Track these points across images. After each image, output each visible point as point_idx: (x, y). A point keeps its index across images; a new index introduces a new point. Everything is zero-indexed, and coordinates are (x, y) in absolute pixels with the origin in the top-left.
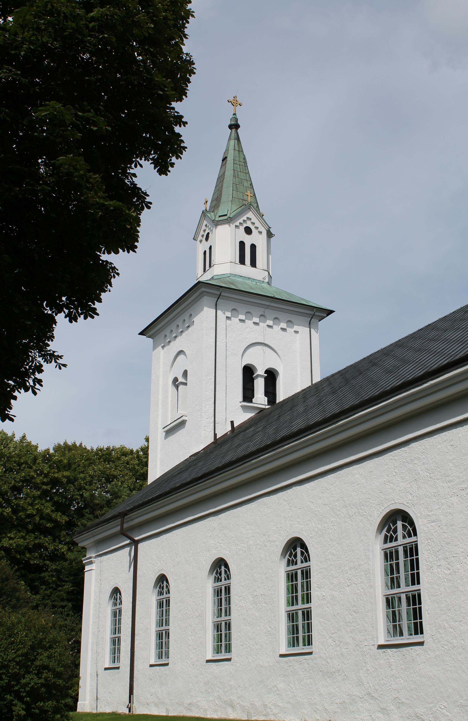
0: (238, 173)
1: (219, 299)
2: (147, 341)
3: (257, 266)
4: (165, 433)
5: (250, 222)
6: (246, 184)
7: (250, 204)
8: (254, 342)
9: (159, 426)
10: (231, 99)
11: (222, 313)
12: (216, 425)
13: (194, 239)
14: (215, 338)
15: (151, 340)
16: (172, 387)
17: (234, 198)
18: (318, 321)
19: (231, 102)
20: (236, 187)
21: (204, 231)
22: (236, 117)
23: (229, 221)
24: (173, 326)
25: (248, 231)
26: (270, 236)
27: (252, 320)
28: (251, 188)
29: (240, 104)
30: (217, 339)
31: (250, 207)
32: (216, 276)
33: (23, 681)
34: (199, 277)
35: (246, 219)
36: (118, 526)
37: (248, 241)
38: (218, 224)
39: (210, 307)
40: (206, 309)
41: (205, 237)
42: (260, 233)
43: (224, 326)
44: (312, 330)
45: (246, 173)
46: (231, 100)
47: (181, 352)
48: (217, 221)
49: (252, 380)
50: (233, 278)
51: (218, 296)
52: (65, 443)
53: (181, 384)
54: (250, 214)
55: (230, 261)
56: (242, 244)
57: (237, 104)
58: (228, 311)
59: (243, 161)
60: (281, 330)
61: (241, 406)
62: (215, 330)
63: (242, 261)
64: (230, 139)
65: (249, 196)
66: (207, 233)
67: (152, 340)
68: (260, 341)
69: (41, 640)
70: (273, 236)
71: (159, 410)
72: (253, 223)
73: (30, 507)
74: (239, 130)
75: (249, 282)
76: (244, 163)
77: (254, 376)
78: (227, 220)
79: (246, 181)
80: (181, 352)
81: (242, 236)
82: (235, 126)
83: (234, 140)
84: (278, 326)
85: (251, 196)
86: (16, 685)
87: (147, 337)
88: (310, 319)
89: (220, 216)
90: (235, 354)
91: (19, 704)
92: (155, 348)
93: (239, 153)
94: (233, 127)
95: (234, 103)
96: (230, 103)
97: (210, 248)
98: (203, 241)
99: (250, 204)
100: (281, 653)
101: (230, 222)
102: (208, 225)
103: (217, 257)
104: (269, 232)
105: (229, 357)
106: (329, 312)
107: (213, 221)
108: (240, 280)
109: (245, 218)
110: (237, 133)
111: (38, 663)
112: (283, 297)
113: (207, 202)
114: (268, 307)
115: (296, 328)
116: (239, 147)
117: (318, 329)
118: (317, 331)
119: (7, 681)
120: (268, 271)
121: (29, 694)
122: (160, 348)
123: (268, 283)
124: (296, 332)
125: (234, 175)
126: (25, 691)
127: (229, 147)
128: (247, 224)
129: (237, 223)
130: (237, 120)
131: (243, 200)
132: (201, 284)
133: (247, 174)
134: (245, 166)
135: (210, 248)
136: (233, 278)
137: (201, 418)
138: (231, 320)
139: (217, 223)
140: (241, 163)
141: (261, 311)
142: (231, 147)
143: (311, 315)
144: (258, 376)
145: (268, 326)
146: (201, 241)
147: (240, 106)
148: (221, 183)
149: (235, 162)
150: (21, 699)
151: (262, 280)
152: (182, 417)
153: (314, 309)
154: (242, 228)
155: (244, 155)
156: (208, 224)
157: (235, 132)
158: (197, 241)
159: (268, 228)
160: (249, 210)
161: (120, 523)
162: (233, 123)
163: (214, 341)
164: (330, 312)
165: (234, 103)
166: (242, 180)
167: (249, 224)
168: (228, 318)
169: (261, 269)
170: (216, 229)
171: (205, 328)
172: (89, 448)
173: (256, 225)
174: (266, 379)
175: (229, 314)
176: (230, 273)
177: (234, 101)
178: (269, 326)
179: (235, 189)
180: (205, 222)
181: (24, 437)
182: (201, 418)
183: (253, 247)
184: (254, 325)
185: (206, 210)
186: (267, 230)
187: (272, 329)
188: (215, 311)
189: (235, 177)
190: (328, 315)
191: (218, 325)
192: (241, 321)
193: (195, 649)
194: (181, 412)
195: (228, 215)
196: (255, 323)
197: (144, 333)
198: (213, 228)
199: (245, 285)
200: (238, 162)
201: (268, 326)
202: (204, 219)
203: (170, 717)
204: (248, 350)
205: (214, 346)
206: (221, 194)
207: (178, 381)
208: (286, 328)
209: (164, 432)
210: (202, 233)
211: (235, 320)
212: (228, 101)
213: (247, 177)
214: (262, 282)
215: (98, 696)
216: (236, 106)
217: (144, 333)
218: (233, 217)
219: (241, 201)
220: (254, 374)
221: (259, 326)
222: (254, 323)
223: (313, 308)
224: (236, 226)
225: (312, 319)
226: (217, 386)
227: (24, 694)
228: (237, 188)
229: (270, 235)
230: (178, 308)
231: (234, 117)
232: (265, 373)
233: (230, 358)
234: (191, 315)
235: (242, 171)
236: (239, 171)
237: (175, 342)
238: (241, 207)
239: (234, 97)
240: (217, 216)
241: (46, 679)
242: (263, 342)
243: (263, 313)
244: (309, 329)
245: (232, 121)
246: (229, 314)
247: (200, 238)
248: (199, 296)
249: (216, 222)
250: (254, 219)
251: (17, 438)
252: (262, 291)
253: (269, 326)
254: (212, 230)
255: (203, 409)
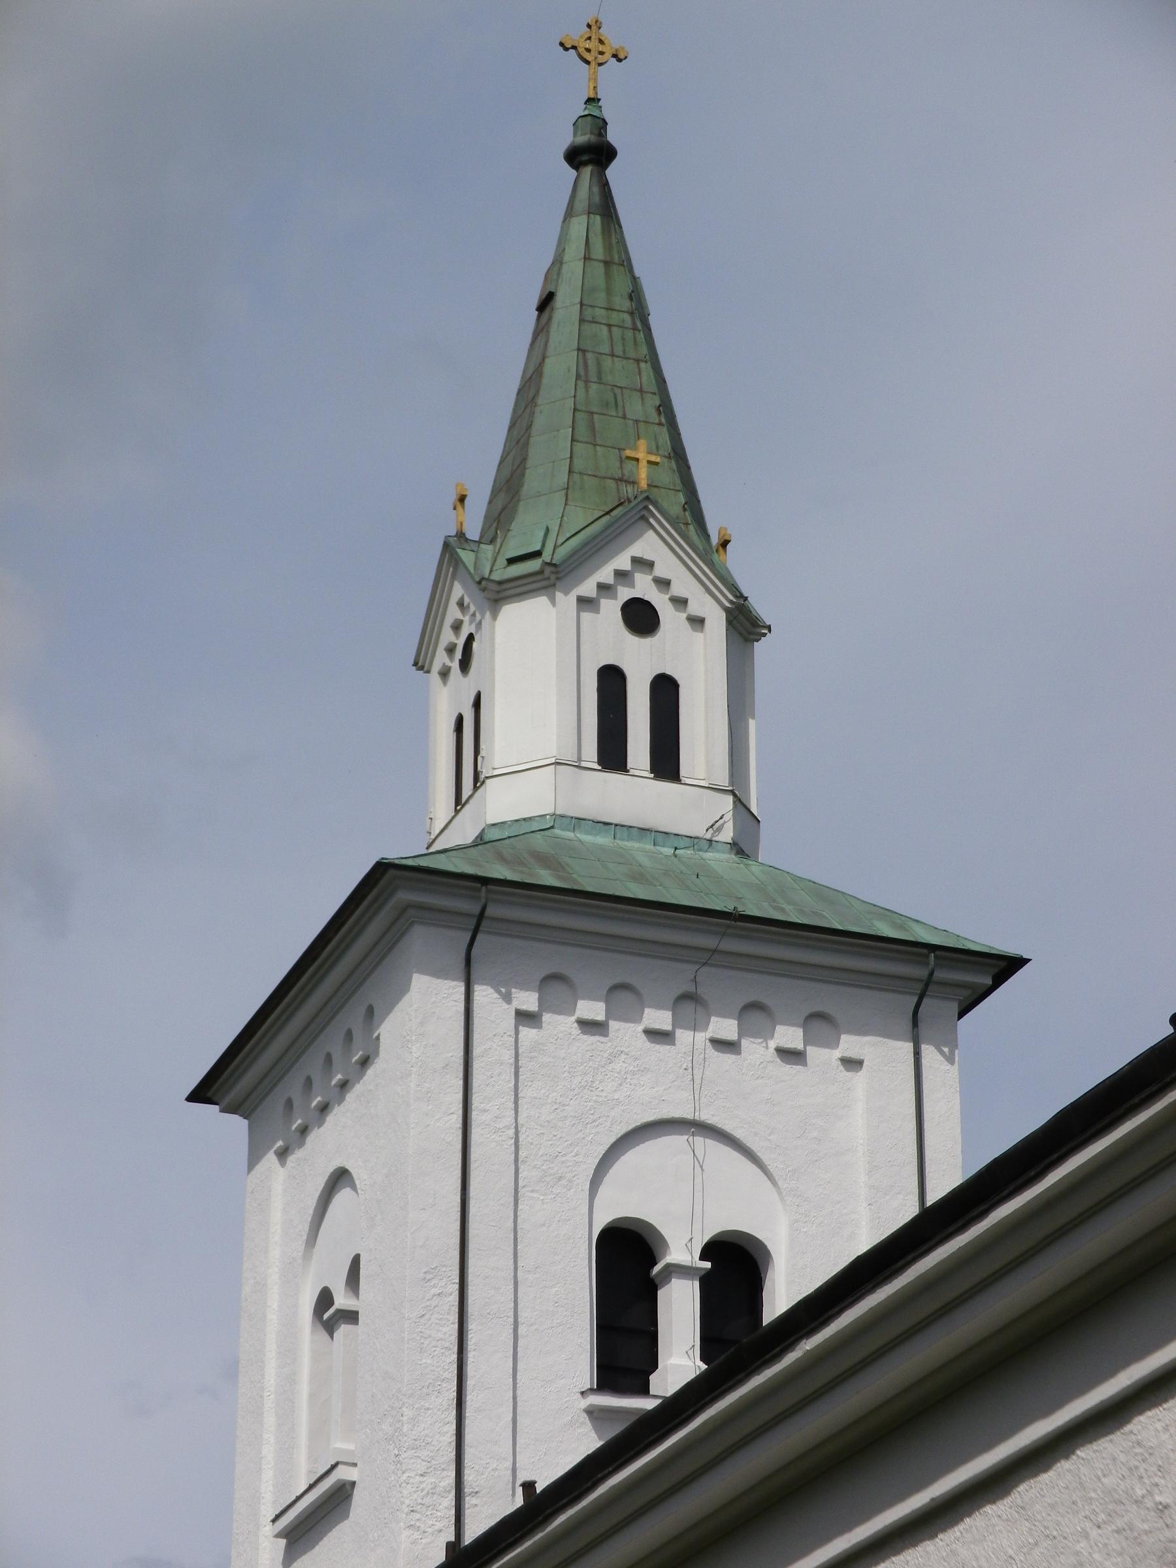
0: (599, 365)
1: (479, 937)
3: (684, 771)
4: (284, 1541)
5: (651, 577)
6: (637, 408)
7: (647, 498)
9: (262, 1507)
10: (577, 33)
11: (496, 995)
12: (469, 1501)
13: (415, 664)
14: (460, 1112)
15: (237, 1125)
16: (313, 1332)
17: (576, 477)
18: (954, 1008)
19: (574, 47)
21: (457, 627)
22: (596, 113)
23: (549, 578)
24: (312, 1064)
26: (750, 633)
27: (638, 1019)
28: (660, 424)
29: (615, 56)
30: (475, 1115)
31: (645, 512)
32: (493, 829)
34: (437, 832)
38: (502, 595)
39: (440, 973)
40: (419, 982)
41: (458, 654)
42: (697, 622)
43: (509, 1056)
44: (928, 1051)
45: (638, 361)
48: (500, 583)
49: (648, 1292)
50: (570, 835)
51: (474, 921)
53: (344, 1317)
54: (648, 545)
55: (553, 760)
57: (602, 53)
58: (524, 986)
59: (626, 304)
60: (778, 1060)
61: (591, 1412)
62: (461, 1075)
64: (570, 213)
65: (643, 464)
66: (466, 636)
67: (246, 1122)
68: (677, 1113)
70: (764, 635)
71: (266, 1436)
72: (663, 584)
75: (638, 848)
76: (632, 314)
77: (657, 1269)
78: (540, 577)
79: (637, 395)
80: (340, 1178)
83: (585, 217)
84: (766, 1041)
85: (649, 462)
87: (222, 1111)
88: (915, 999)
89: (512, 561)
90: (560, 1178)
93: (608, 275)
94: (585, 158)
95: (588, 50)
96: (572, 51)
97: (477, 704)
98: (452, 671)
99: (647, 498)
101: (554, 585)
102: (467, 600)
104: (741, 617)
105: (532, 1191)
106: (1003, 964)
107: (479, 583)
108: (602, 840)
109: (622, 562)
112: (783, 910)
114: (710, 958)
115: (850, 1044)
116: (608, 247)
117: (956, 1046)
118: (952, 1053)
120: (732, 792)
122: (271, 1158)
123: (738, 849)
125: (582, 373)
127: (564, 249)
128: (633, 587)
129: (588, 588)
130: (601, 125)
131: (621, 480)
132: (392, 872)
133: (643, 365)
134: (635, 329)
135: (477, 704)
136: (570, 835)
137: (399, 1473)
140: (615, 318)
141: (680, 978)
142: (575, 250)
143: (919, 980)
144: (674, 1270)
146: (445, 674)
147: (620, 60)
148: (528, 411)
149: (588, 313)
151: (699, 830)
152: (333, 1467)
153: (927, 956)
154: (611, 609)
155: (635, 279)
156: (465, 596)
157: (595, 180)
158: (428, 672)
159: (731, 597)
160: (642, 524)
162: (582, 139)
163: (459, 1124)
166: (618, 391)
167: (643, 587)
168: (525, 1018)
169: (702, 783)
170: (495, 616)
171: (414, 1069)
173: (677, 590)
174: (707, 1282)
175: (528, 1000)
176: (551, 811)
178: (720, 1044)
179: (582, 431)
180: (458, 591)
182: (399, 1473)
184: (648, 1044)
185: (461, 535)
186: (727, 610)
187: (733, 1057)
188: (461, 988)
189: (587, 382)
190: (1000, 979)
191: (477, 1051)
192: (589, 1026)
194: (342, 1445)
195: (546, 556)
197: (209, 1094)
198: (483, 616)
199: (611, 866)
200: (600, 313)
202: (454, 577)
204: (623, 1158)
205: (459, 1146)
206: (524, 460)
207: (331, 1303)
208: (800, 1046)
209: (278, 1536)
210: (447, 636)
211: (559, 1025)
212: (562, 44)
213: (644, 378)
214: (705, 845)
216: (600, 65)
217: (209, 1094)
218: (564, 561)
219: (611, 484)
220: (654, 1263)
221: (674, 1044)
223: (925, 951)
225: (926, 1001)
230: (321, 980)
231: (586, 113)
233: (535, 1195)
234: (370, 1011)
235: (618, 350)
236: (607, 351)
237: (322, 1129)
238: (608, 513)
239: (589, 26)
240: (501, 561)
242: (690, 1116)
243: (690, 988)
244: (909, 1046)
245: (579, 133)
246: (528, 1000)
247: (441, 659)
248: (393, 924)
249: (496, 587)
250: (667, 564)
252: (688, 888)
253: (720, 1044)
254: (480, 623)
255: (405, 1429)
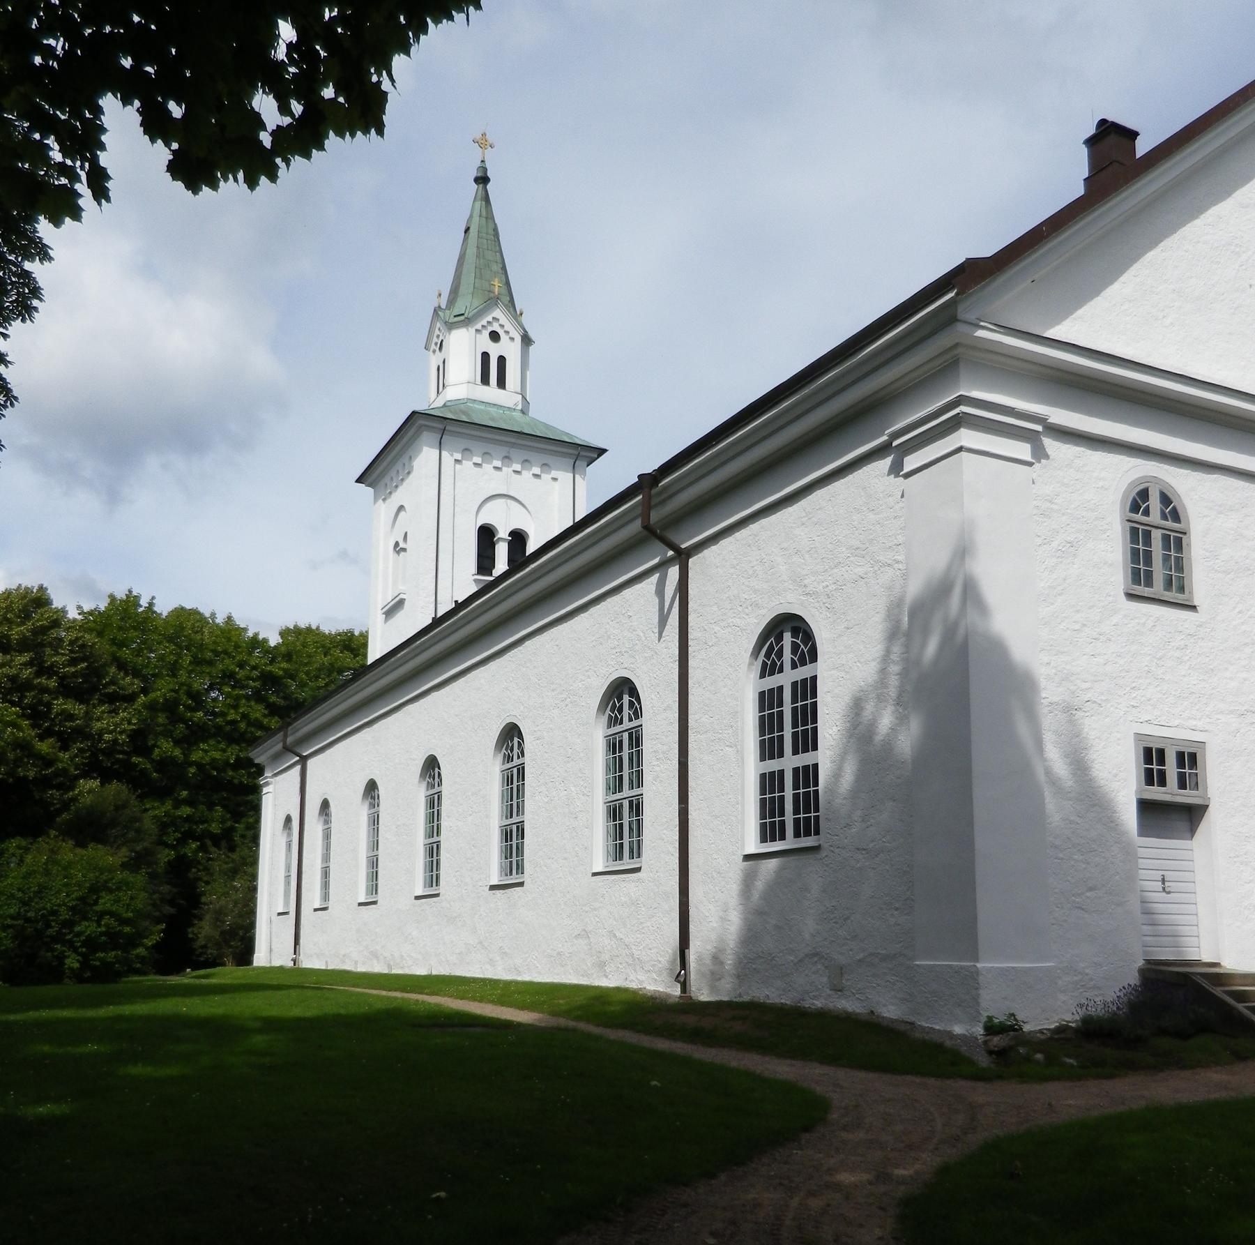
2: (366, 491)
3: (507, 387)
8: (494, 494)
12: (439, 606)
15: (370, 490)
20: (479, 273)
25: (495, 336)
27: (491, 463)
33: (77, 929)
35: (491, 320)
36: (278, 743)
37: (495, 351)
40: (426, 449)
42: (512, 339)
44: (577, 476)
46: (478, 138)
47: (401, 508)
49: (492, 546)
52: (296, 626)
54: (497, 313)
56: (485, 356)
63: (485, 380)
69: (106, 882)
72: (502, 326)
73: (232, 711)
74: (488, 187)
77: (495, 539)
80: (401, 508)
81: (486, 344)
82: (482, 180)
86: (69, 934)
89: (455, 316)
91: (73, 955)
92: (376, 500)
93: (487, 221)
100: (360, 901)
103: (453, 375)
108: (482, 407)
109: (490, 318)
110: (486, 191)
111: (98, 908)
113: (440, 295)
114: (514, 445)
115: (554, 473)
116: (487, 212)
119: (57, 929)
121: (84, 944)
123: (523, 412)
124: (555, 479)
126: (79, 941)
129: (479, 326)
130: (485, 169)
134: (495, 241)
138: (462, 464)
139: (451, 326)
141: (504, 451)
142: (476, 213)
144: (500, 539)
145: (514, 471)
146: (434, 351)
150: (75, 950)
151: (511, 405)
154: (486, 334)
155: (495, 224)
161: (281, 738)
162: (479, 175)
164: (602, 451)
165: (483, 142)
167: (496, 327)
170: (450, 334)
172: (327, 632)
174: (510, 543)
177: (482, 142)
180: (438, 325)
181: (229, 618)
183: (502, 360)
185: (439, 307)
190: (599, 455)
193: (350, 890)
194: (401, 588)
195: (466, 315)
196: (496, 468)
201: (514, 471)
203: (329, 970)
209: (383, 614)
210: (435, 340)
211: (467, 464)
215: (273, 947)
220: (494, 537)
222: (495, 468)
224: (477, 330)
226: (440, 554)
227: (79, 944)
228: (481, 274)
229: (527, 340)
232: (509, 536)
234: (411, 457)
235: (490, 248)
240: (452, 316)
241: (107, 925)
243: (507, 455)
246: (458, 456)
247: (433, 346)
251: (220, 620)
